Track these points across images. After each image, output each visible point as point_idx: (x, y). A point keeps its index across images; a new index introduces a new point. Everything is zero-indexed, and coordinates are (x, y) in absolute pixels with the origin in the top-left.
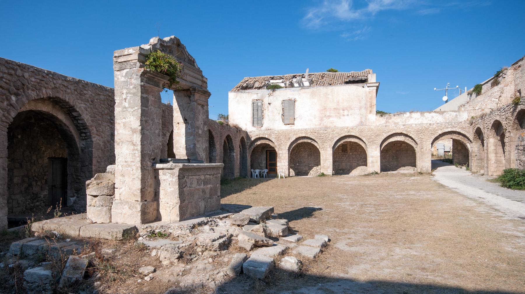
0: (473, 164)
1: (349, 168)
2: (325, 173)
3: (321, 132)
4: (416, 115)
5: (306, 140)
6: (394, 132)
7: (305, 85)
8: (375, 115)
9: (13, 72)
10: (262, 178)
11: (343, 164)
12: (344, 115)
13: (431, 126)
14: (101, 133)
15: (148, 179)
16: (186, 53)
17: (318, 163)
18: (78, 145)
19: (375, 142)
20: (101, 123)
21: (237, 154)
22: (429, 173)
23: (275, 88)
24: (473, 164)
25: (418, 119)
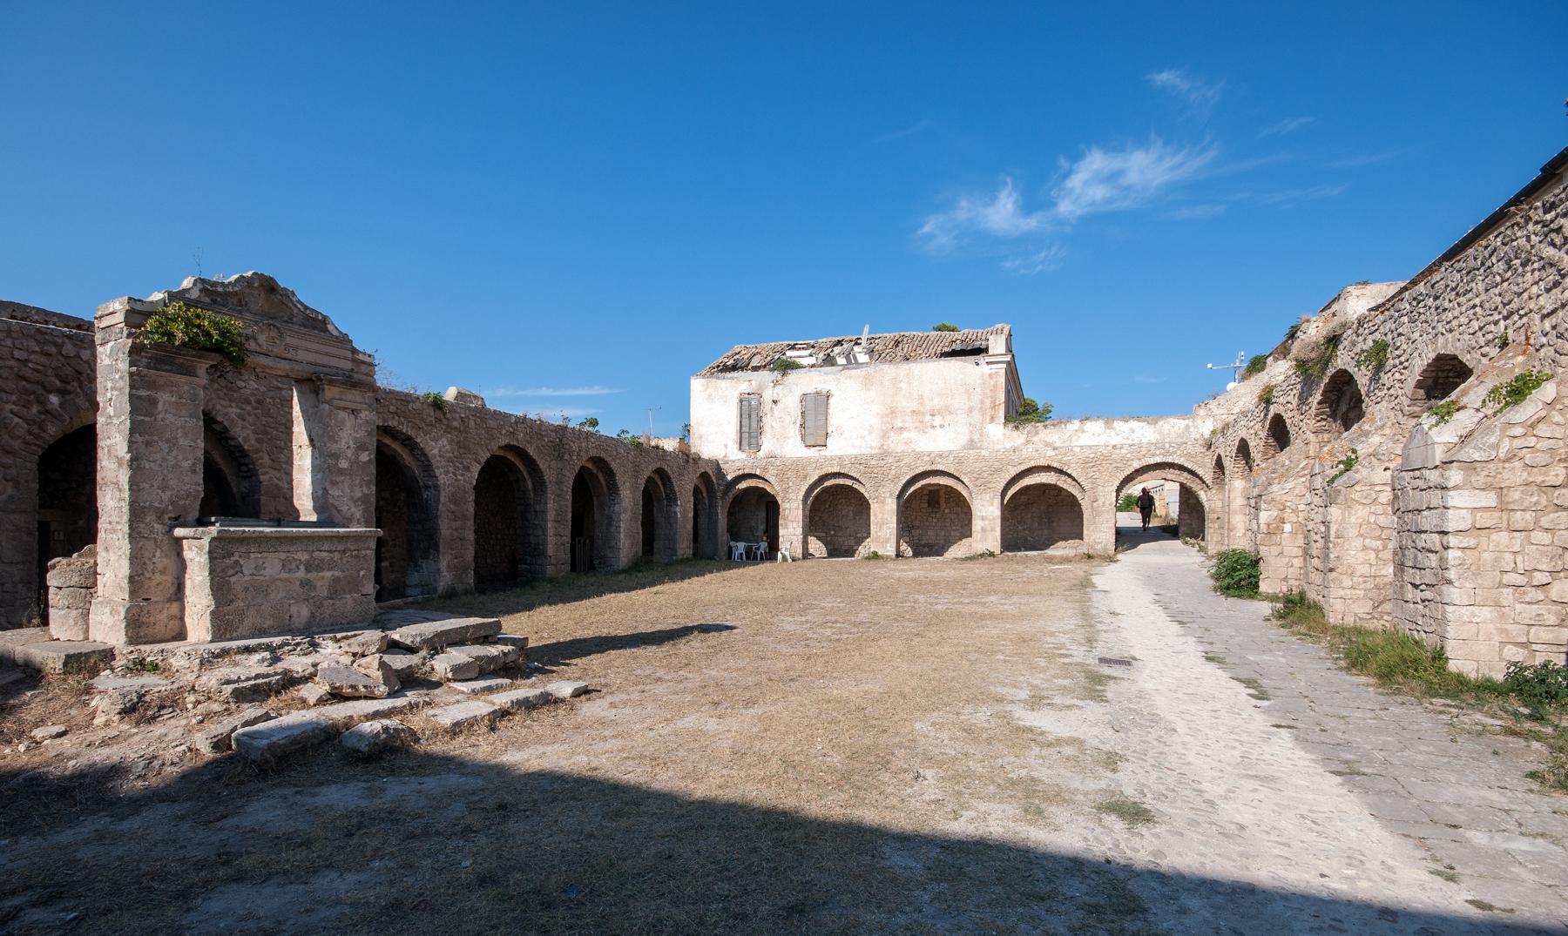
0: (1212, 537)
1: (942, 542)
2: (880, 553)
3: (873, 462)
4: (1095, 427)
5: (841, 481)
6: (1033, 464)
7: (860, 361)
8: (1002, 426)
9: (53, 350)
10: (751, 557)
11: (930, 533)
12: (933, 427)
13: (1117, 451)
14: (284, 466)
15: (154, 556)
16: (296, 306)
17: (965, 531)
18: (235, 489)
19: (989, 485)
20: (283, 444)
21: (684, 508)
22: (1109, 557)
23: (787, 367)
24: (1212, 537)
25: (1099, 435)
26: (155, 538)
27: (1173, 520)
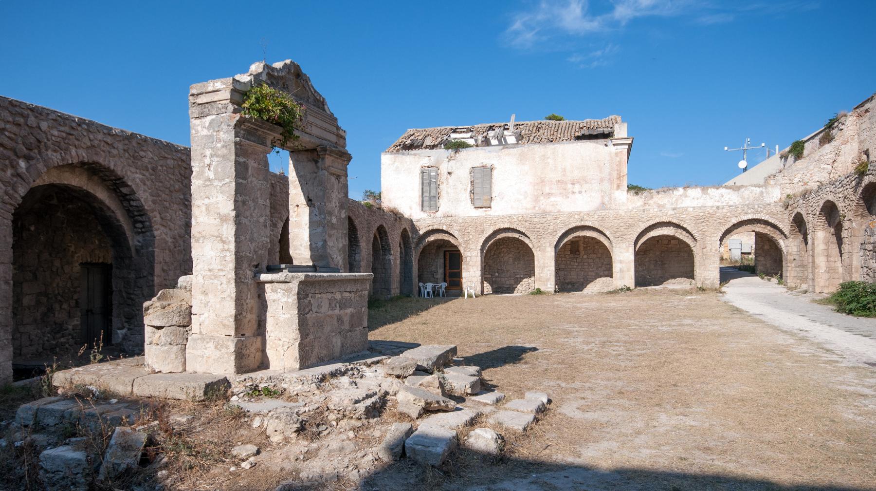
0: (790, 274)
2: (542, 290)
3: (536, 220)
4: (695, 193)
5: (510, 235)
6: (657, 220)
7: (509, 143)
8: (625, 192)
9: (22, 120)
10: (437, 297)
11: (573, 274)
12: (573, 193)
13: (720, 211)
14: (169, 223)
17: (530, 272)
18: (131, 243)
19: (625, 237)
20: (168, 205)
22: (716, 290)
23: (459, 146)
24: (790, 274)
25: (698, 199)
26: (247, 283)
27: (737, 261)
